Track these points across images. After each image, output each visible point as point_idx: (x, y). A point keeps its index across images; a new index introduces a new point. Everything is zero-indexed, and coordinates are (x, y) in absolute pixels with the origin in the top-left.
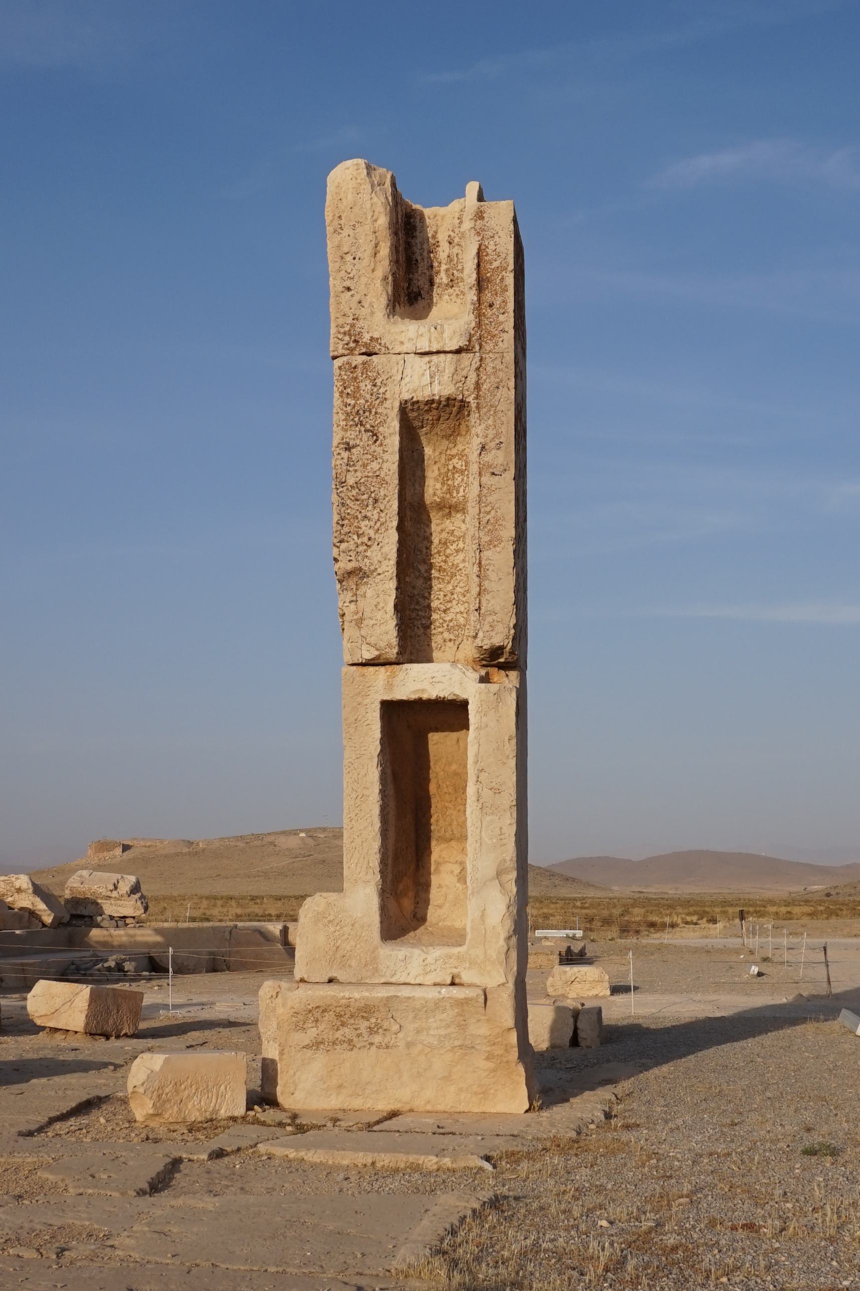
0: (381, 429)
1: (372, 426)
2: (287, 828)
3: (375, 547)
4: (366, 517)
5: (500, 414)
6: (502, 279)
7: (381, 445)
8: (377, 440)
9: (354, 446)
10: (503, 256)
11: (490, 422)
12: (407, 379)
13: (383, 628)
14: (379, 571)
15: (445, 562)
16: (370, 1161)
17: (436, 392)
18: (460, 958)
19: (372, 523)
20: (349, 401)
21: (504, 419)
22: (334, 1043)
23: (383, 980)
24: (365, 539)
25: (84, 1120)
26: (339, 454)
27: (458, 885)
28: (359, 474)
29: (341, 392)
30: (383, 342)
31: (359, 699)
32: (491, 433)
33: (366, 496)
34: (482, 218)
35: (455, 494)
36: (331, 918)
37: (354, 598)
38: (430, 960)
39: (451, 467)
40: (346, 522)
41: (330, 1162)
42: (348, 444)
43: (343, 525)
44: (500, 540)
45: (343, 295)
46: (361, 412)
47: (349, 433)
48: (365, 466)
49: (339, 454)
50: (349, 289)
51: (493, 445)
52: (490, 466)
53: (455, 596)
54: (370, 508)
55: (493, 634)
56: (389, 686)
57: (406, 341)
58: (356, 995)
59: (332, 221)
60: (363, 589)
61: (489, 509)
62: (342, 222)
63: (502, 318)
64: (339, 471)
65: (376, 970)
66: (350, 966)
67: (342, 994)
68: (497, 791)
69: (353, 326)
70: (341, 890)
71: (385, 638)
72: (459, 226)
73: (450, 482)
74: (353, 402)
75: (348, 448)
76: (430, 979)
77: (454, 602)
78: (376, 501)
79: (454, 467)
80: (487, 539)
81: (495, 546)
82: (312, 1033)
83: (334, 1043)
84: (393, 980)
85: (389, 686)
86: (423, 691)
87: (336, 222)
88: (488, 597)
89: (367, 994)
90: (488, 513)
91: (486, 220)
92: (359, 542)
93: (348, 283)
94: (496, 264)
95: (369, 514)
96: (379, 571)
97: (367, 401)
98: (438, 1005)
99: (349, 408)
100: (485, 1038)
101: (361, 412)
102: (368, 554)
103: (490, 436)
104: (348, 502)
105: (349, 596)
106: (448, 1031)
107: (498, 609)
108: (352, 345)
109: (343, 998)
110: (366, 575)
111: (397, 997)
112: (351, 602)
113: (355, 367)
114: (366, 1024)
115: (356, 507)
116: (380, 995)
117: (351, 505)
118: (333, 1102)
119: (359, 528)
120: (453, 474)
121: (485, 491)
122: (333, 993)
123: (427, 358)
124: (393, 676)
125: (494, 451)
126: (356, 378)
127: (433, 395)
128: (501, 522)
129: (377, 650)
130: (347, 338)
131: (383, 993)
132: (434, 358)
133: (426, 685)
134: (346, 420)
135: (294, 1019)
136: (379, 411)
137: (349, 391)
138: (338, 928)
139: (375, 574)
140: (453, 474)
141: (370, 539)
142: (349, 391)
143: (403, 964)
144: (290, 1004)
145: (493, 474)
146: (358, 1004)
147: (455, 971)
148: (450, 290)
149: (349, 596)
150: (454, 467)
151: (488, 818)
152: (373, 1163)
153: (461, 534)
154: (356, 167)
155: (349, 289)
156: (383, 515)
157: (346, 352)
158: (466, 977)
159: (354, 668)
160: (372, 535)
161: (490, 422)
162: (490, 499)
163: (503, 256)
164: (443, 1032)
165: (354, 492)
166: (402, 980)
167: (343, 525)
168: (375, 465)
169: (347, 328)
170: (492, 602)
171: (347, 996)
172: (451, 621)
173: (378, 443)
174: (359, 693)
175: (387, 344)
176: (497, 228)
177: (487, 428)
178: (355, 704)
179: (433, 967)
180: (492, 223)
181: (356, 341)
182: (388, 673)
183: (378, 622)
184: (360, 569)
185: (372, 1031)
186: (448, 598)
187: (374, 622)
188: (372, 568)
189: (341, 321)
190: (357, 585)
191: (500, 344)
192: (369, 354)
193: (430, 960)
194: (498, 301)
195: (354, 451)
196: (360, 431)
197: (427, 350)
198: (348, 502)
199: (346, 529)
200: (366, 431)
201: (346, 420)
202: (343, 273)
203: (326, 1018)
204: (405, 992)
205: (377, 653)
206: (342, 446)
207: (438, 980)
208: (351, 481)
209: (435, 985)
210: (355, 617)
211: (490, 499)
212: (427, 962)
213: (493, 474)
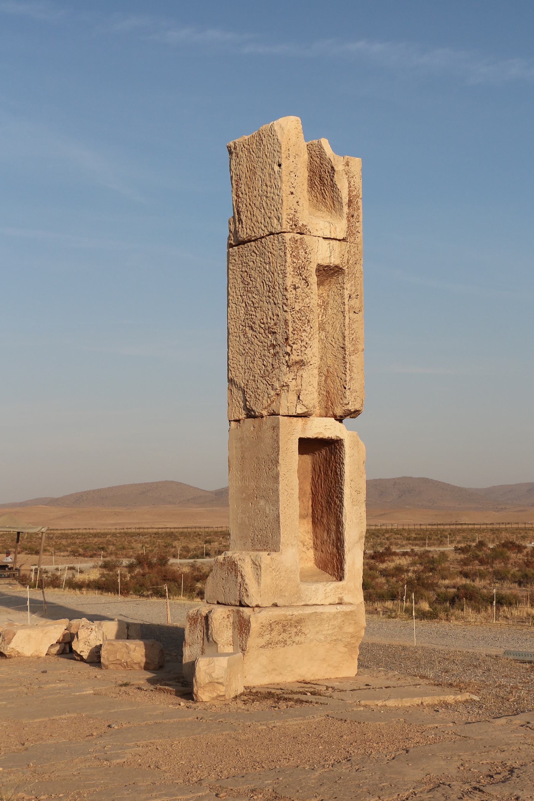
0: (309, 279)
1: (306, 277)
3: (308, 349)
4: (304, 330)
5: (357, 279)
7: (309, 289)
8: (308, 285)
9: (298, 287)
10: (358, 189)
11: (353, 282)
12: (320, 252)
13: (312, 396)
14: (311, 363)
16: (420, 702)
17: (332, 262)
18: (343, 588)
19: (307, 334)
22: (277, 643)
23: (303, 603)
24: (304, 343)
26: (291, 291)
28: (300, 304)
29: (291, 254)
30: (308, 228)
31: (289, 436)
32: (354, 289)
33: (304, 318)
34: (348, 165)
36: (274, 567)
37: (295, 377)
38: (328, 590)
40: (295, 332)
41: (400, 706)
42: (295, 286)
43: (294, 334)
45: (289, 196)
46: (300, 268)
47: (295, 279)
48: (303, 300)
49: (291, 291)
50: (292, 193)
52: (353, 308)
54: (306, 325)
55: (356, 403)
56: (304, 430)
57: (319, 230)
58: (296, 613)
59: (285, 151)
60: (301, 372)
61: (353, 332)
62: (290, 153)
64: (292, 302)
65: (299, 598)
66: (285, 596)
67: (288, 613)
68: (359, 493)
69: (294, 215)
70: (276, 549)
71: (313, 402)
75: (295, 289)
76: (327, 602)
78: (309, 321)
82: (267, 637)
83: (277, 643)
84: (309, 603)
85: (304, 430)
86: (321, 433)
87: (287, 152)
88: (353, 382)
89: (301, 612)
90: (353, 334)
91: (350, 167)
93: (292, 190)
95: (306, 329)
96: (311, 363)
97: (303, 262)
98: (335, 616)
99: (295, 265)
100: (351, 633)
101: (300, 268)
102: (306, 352)
103: (353, 291)
104: (296, 320)
105: (292, 376)
106: (334, 631)
107: (357, 389)
108: (294, 227)
109: (289, 615)
110: (304, 364)
111: (316, 612)
112: (293, 379)
114: (295, 630)
115: (300, 324)
116: (307, 612)
117: (297, 322)
118: (266, 680)
119: (302, 336)
121: (351, 322)
122: (284, 613)
123: (327, 241)
124: (305, 424)
126: (298, 247)
127: (331, 263)
128: (358, 340)
129: (307, 408)
131: (309, 610)
132: (331, 241)
133: (322, 430)
134: (293, 271)
135: (260, 630)
137: (294, 254)
138: (277, 573)
139: (309, 364)
141: (306, 343)
142: (294, 254)
143: (314, 593)
144: (260, 621)
145: (355, 312)
146: (297, 618)
147: (340, 596)
149: (292, 376)
151: (355, 508)
152: (422, 703)
154: (297, 122)
155: (292, 193)
156: (312, 330)
157: (291, 230)
158: (346, 599)
159: (286, 418)
160: (308, 341)
161: (353, 282)
162: (354, 326)
163: (358, 189)
164: (330, 632)
165: (299, 315)
166: (314, 603)
167: (294, 334)
168: (307, 300)
169: (291, 216)
171: (291, 614)
173: (308, 287)
174: (289, 433)
175: (310, 230)
176: (355, 173)
177: (351, 286)
178: (287, 439)
179: (329, 594)
180: (352, 169)
181: (295, 225)
182: (303, 422)
183: (309, 393)
184: (302, 361)
185: (297, 634)
187: (307, 392)
188: (308, 361)
189: (289, 211)
190: (298, 370)
191: (357, 238)
193: (328, 590)
195: (297, 290)
196: (300, 279)
197: (329, 237)
198: (296, 320)
199: (296, 336)
200: (303, 279)
201: (293, 271)
202: (290, 184)
203: (277, 628)
204: (320, 609)
205: (306, 410)
207: (332, 602)
208: (297, 308)
209: (330, 604)
210: (297, 389)
211: (354, 326)
212: (327, 591)
213: (355, 312)
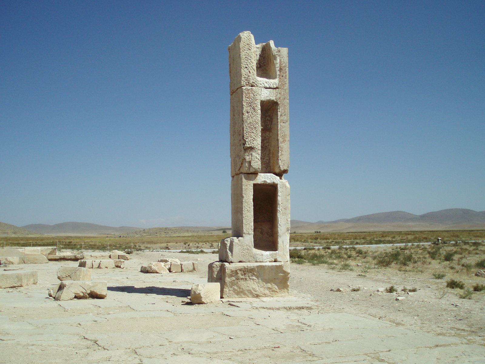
2: (361, 231)
6: (285, 70)
15: (264, 145)
20: (247, 99)
21: (286, 108)
24: (253, 138)
25: (299, 312)
27: (260, 235)
35: (267, 127)
39: (267, 119)
42: (247, 111)
44: (285, 141)
51: (283, 114)
53: (266, 155)
55: (284, 166)
63: (285, 80)
72: (282, 55)
73: (266, 123)
74: (248, 100)
77: (266, 157)
79: (267, 119)
80: (282, 140)
81: (284, 142)
90: (282, 133)
92: (251, 139)
94: (283, 65)
95: (254, 132)
113: (249, 90)
120: (267, 121)
125: (284, 116)
130: (246, 81)
136: (255, 103)
140: (267, 121)
145: (284, 122)
148: (260, 69)
150: (267, 119)
153: (268, 138)
162: (283, 129)
163: (285, 63)
170: (284, 158)
172: (265, 161)
180: (282, 54)
186: (264, 155)
187: (254, 162)
192: (252, 86)
194: (284, 75)
198: (248, 128)
205: (255, 170)
206: (246, 112)
211: (283, 129)
213: (284, 122)
